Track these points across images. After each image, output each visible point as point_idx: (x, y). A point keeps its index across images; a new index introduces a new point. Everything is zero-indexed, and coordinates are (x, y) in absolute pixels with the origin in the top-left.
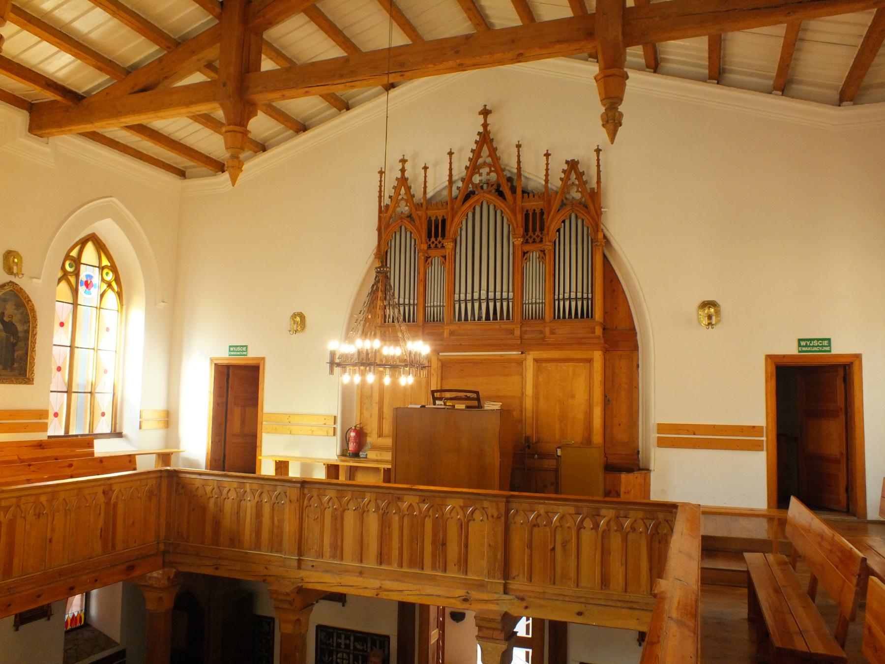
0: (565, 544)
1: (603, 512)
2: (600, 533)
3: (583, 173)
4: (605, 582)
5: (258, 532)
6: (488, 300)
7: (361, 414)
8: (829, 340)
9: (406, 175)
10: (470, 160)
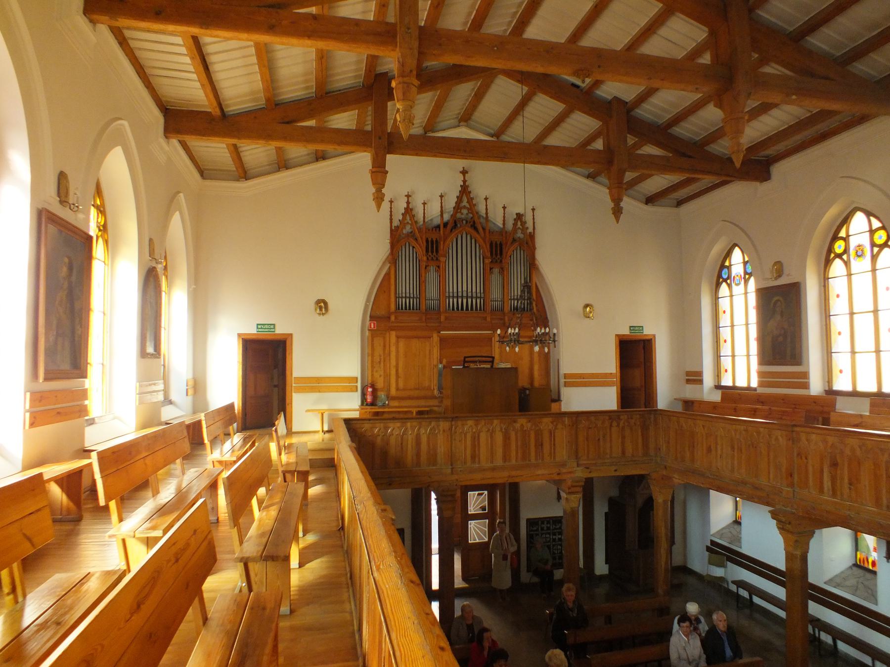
1: (622, 417)
4: (623, 453)
5: (418, 454)
7: (372, 375)
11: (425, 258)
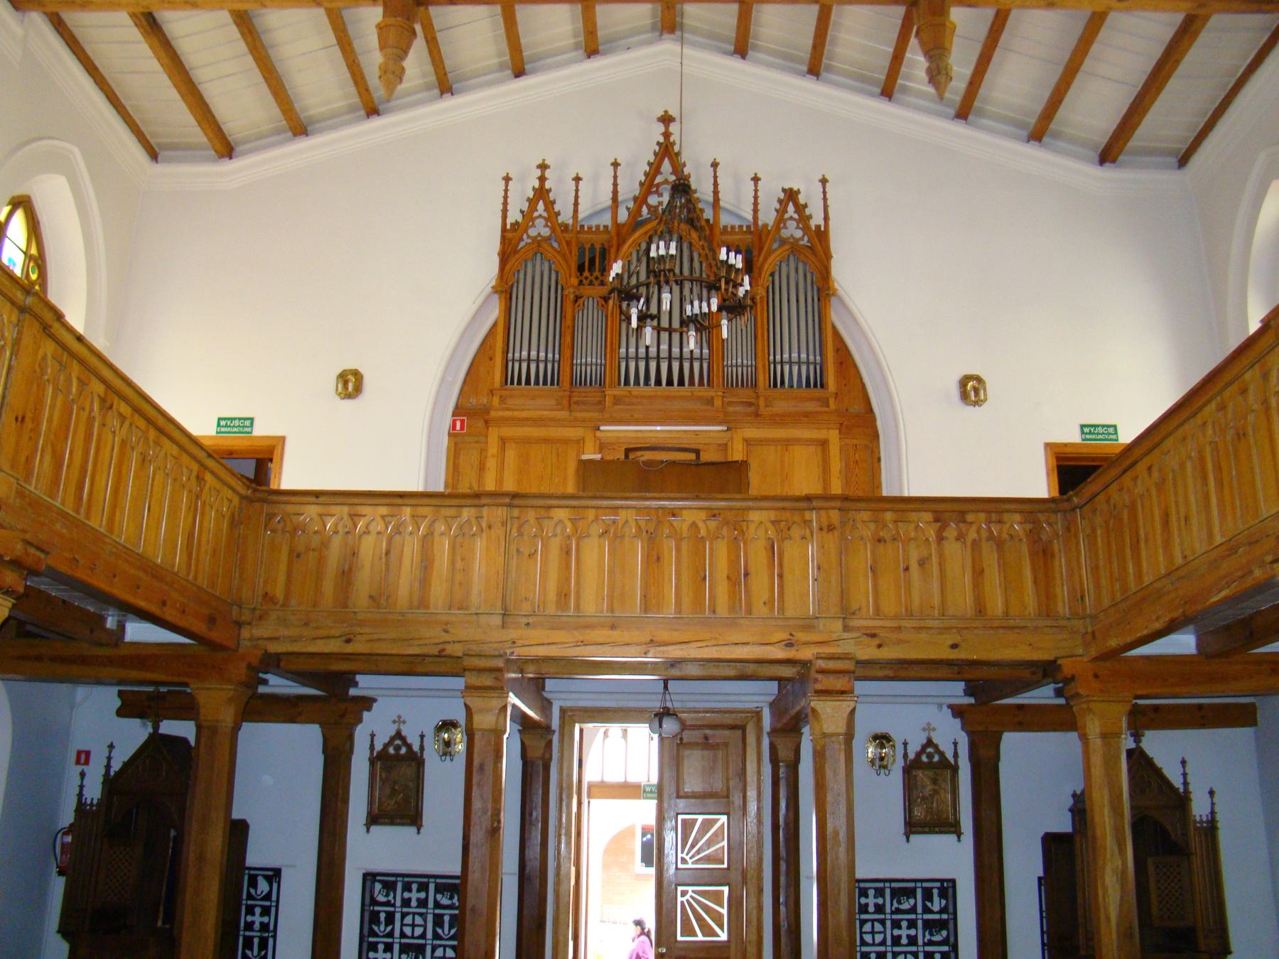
0: (922, 563)
2: (969, 544)
3: (805, 206)
6: (670, 358)
8: (1115, 427)
9: (547, 185)
10: (646, 174)
11: (575, 281)
